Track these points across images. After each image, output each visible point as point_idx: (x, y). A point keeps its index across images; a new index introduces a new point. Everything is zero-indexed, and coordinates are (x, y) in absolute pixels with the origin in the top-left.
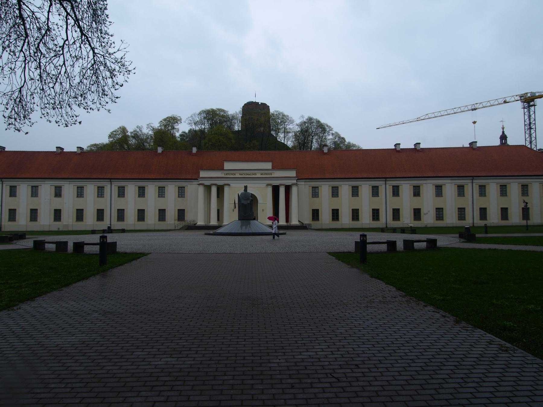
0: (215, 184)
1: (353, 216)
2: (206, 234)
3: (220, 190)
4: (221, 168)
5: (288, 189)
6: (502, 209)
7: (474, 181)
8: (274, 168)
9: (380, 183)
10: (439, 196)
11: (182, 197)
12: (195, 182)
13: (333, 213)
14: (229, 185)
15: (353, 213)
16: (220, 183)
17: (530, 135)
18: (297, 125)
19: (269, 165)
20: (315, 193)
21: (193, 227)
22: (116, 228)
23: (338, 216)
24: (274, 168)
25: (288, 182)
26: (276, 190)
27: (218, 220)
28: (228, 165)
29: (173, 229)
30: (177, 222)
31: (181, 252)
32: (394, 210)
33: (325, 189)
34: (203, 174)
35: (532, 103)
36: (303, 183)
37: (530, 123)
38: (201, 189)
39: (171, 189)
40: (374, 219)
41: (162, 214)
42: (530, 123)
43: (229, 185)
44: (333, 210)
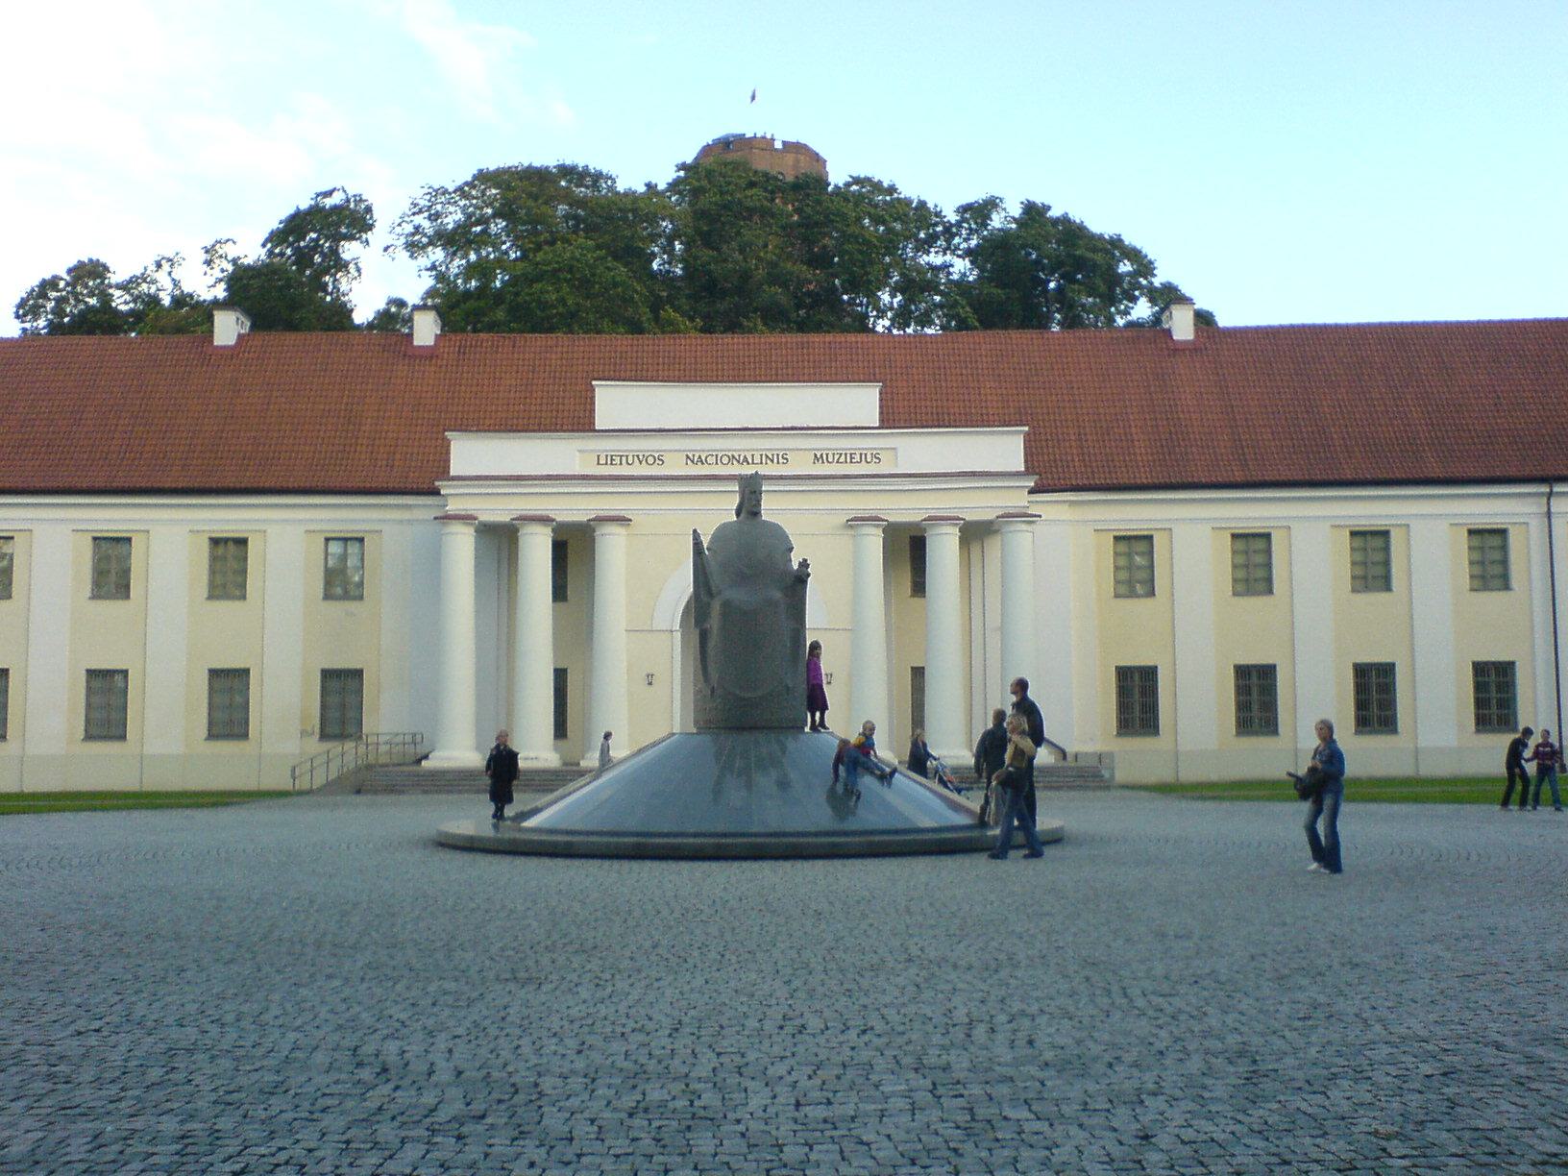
0: (544, 520)
3: (573, 550)
4: (580, 421)
7: (1558, 506)
8: (890, 418)
10: (227, 596)
11: (346, 596)
12: (421, 509)
13: (1123, 692)
14: (622, 520)
16: (573, 509)
19: (861, 402)
20: (1135, 564)
21: (405, 775)
22: (1278, 807)
23: (1270, 705)
24: (890, 418)
25: (980, 505)
26: (909, 549)
27: (561, 730)
28: (617, 403)
29: (286, 784)
30: (314, 746)
34: (468, 454)
36: (1024, 527)
38: (462, 544)
39: (286, 534)
41: (228, 696)
43: (622, 520)
44: (1124, 674)
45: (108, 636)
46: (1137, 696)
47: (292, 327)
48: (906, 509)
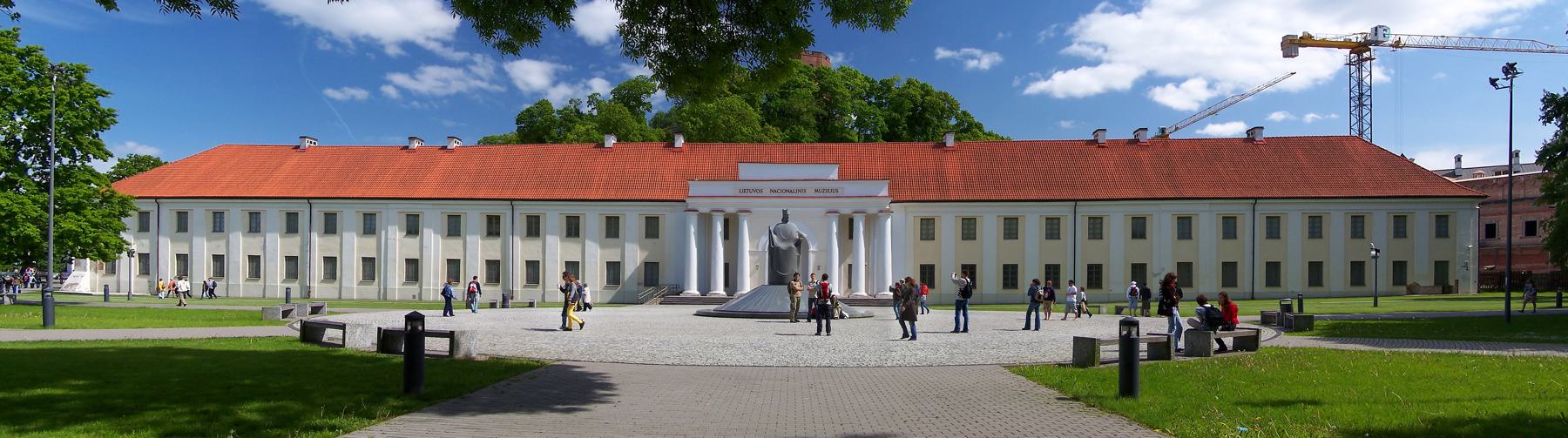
1: (1005, 279)
2: (699, 314)
5: (873, 222)
6: (1311, 264)
9: (1061, 210)
15: (1005, 273)
16: (731, 207)
17: (1361, 119)
18: (112, 271)
20: (927, 229)
24: (842, 177)
28: (745, 170)
31: (689, 362)
32: (1090, 267)
33: (948, 219)
34: (696, 188)
35: (1366, 55)
37: (1361, 95)
38: (693, 218)
40: (1006, 286)
42: (1361, 95)
44: (1006, 267)
45: (1316, 251)
46: (51, 264)
47: (541, 141)
48: (846, 208)
